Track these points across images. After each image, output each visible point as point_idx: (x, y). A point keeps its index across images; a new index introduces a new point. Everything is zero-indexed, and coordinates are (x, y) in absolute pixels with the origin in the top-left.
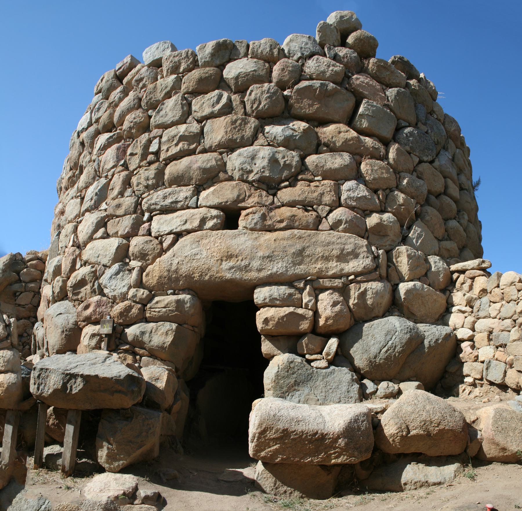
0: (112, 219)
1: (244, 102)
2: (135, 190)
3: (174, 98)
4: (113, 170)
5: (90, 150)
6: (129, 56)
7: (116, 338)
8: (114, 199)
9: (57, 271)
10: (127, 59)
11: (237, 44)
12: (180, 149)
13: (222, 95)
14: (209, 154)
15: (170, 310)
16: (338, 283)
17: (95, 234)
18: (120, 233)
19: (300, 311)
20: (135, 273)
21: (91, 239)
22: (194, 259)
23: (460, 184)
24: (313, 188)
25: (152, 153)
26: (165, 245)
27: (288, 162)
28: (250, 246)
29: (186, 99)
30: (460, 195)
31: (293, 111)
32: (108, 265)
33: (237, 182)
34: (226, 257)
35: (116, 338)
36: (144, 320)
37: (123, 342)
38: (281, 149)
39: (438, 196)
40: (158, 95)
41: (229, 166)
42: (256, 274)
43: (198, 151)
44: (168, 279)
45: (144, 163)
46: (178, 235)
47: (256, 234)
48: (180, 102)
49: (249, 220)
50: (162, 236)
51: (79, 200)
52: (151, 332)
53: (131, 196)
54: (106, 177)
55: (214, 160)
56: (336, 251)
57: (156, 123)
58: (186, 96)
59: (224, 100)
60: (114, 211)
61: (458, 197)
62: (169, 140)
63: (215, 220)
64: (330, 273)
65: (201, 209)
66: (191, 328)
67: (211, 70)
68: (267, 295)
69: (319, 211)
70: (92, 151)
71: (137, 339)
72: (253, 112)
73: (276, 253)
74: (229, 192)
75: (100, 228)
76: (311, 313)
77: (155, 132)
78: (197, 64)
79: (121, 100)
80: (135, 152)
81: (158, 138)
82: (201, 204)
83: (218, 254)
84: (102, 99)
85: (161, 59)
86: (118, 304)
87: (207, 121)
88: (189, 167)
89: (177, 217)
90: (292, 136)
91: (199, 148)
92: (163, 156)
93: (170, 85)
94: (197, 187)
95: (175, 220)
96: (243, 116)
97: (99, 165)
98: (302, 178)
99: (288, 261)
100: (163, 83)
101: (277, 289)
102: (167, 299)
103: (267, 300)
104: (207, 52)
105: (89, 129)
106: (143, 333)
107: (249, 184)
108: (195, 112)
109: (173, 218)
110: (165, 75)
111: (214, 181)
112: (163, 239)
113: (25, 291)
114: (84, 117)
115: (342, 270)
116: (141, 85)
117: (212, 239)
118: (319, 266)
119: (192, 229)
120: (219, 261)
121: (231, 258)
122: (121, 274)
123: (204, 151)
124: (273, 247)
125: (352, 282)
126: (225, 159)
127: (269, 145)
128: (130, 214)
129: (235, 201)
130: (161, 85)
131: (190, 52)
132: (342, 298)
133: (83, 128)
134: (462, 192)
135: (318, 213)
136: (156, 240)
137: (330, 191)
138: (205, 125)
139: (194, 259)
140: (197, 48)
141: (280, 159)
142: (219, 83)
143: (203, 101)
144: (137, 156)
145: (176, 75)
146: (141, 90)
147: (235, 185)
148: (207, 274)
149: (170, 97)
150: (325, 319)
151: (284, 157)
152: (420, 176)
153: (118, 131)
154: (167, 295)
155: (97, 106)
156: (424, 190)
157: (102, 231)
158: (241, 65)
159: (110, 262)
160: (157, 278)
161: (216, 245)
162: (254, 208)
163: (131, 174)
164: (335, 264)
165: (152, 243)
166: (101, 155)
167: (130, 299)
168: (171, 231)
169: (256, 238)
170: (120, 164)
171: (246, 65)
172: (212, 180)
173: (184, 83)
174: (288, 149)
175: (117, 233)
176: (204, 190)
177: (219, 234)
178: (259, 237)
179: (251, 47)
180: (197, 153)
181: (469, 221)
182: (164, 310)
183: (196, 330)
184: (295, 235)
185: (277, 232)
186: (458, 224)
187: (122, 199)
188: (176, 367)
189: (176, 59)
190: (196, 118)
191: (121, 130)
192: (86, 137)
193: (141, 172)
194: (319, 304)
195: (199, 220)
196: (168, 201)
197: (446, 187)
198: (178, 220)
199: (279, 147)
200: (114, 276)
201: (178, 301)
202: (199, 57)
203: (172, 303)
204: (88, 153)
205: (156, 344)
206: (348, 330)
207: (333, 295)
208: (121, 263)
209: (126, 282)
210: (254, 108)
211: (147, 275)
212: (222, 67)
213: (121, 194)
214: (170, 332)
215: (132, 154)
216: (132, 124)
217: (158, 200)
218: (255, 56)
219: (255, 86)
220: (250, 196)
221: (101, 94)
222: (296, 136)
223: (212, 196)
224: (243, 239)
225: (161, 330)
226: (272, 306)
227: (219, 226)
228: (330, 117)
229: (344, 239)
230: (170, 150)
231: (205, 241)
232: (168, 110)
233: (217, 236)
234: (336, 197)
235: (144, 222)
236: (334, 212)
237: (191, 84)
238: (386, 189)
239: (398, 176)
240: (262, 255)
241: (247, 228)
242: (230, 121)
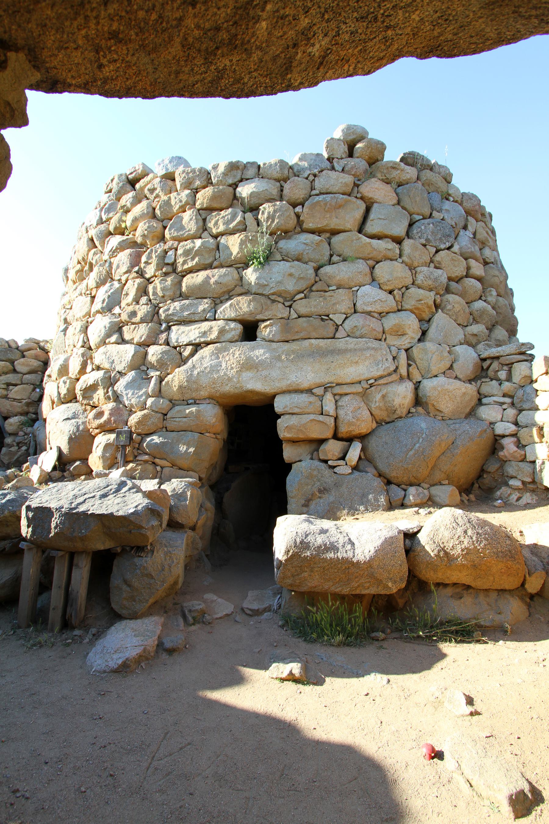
0: (127, 325)
9: (64, 370)
16: (358, 389)
20: (153, 381)
21: (103, 342)
23: (484, 260)
30: (485, 271)
31: (305, 226)
35: (134, 448)
37: (142, 453)
39: (458, 280)
46: (197, 347)
48: (194, 218)
50: (180, 346)
51: (89, 298)
53: (147, 304)
54: (119, 280)
59: (239, 219)
61: (483, 274)
66: (214, 436)
93: (184, 199)
95: (193, 331)
112: (182, 350)
113: (22, 384)
134: (487, 266)
152: (437, 265)
156: (444, 280)
161: (235, 357)
166: (113, 257)
175: (133, 339)
181: (499, 295)
183: (219, 436)
186: (485, 304)
187: (138, 306)
197: (468, 268)
202: (212, 176)
206: (370, 433)
213: (137, 301)
228: (342, 228)
238: (402, 287)
239: (414, 272)
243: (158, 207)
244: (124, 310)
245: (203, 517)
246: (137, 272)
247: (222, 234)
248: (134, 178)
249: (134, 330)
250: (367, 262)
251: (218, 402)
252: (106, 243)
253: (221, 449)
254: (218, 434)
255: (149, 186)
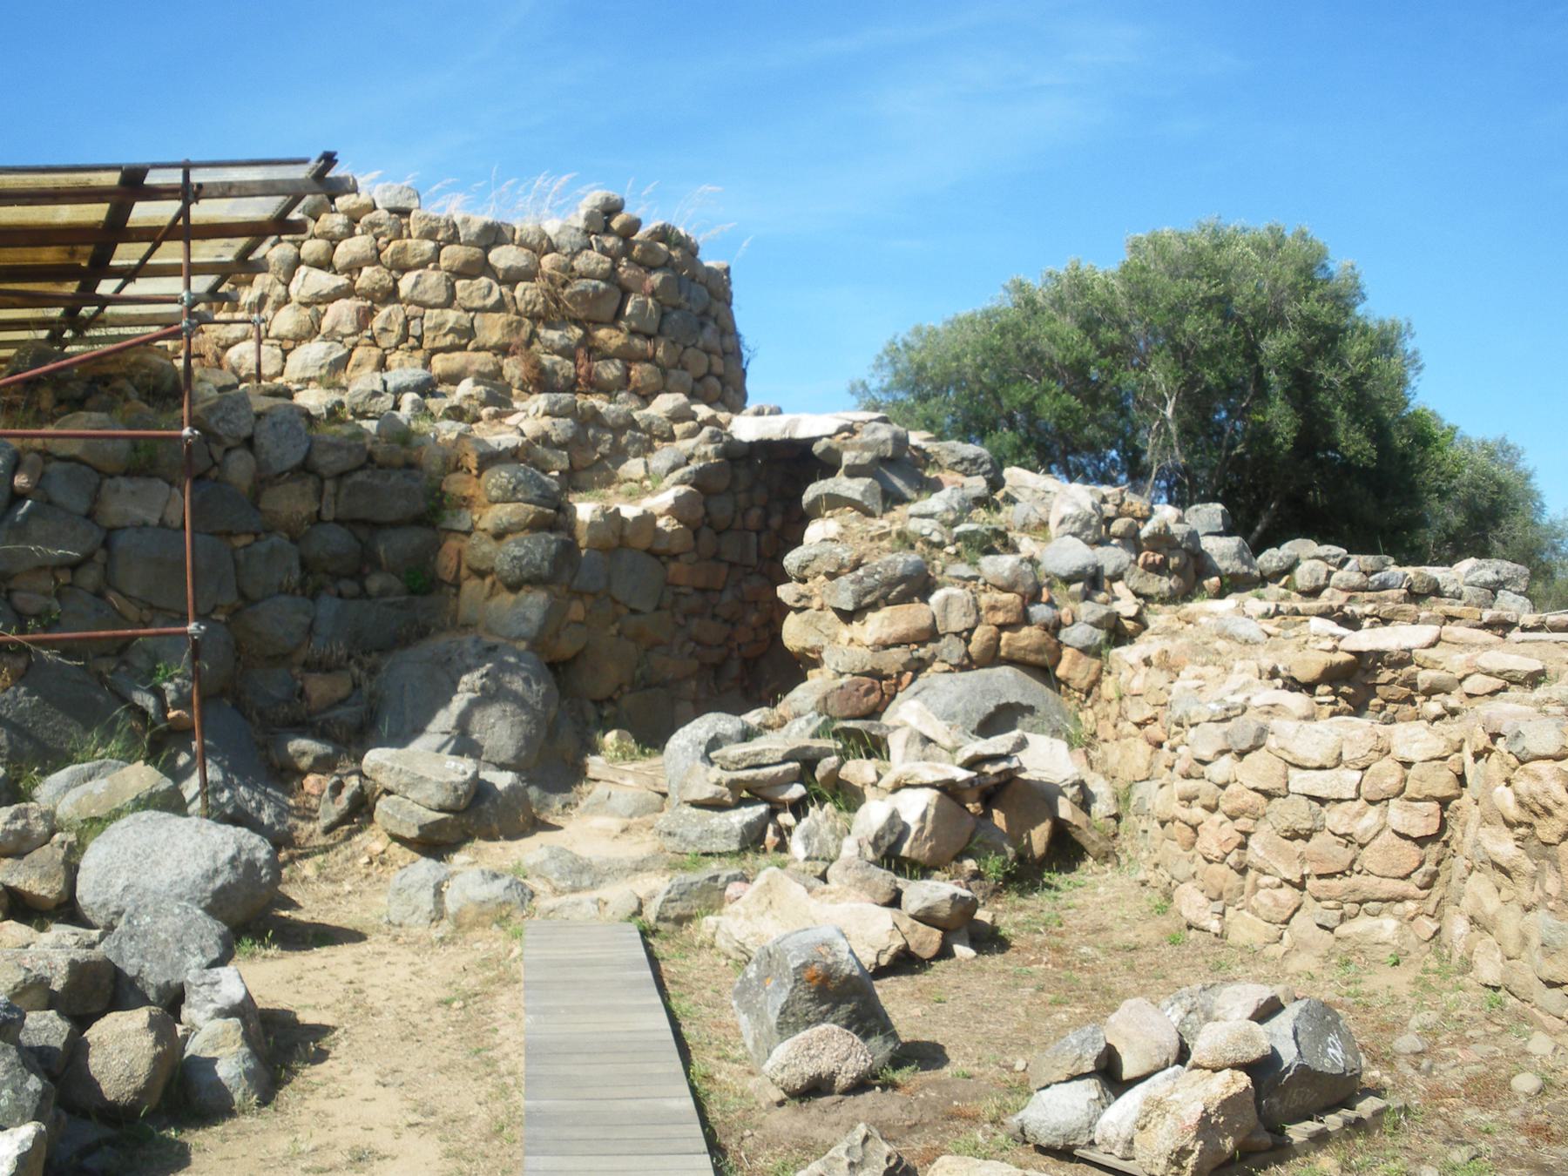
59: (495, 296)
92: (427, 344)
123: (477, 349)
189: (434, 224)
197: (710, 365)
212: (487, 249)
218: (523, 244)
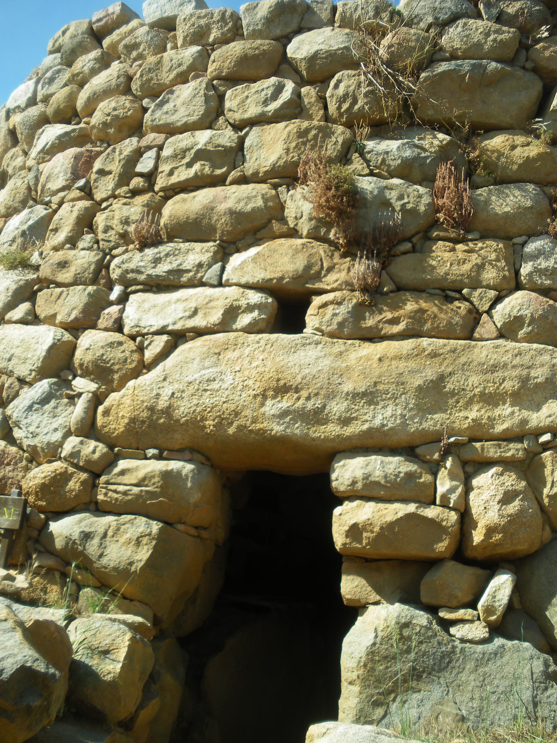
0: (48, 287)
1: (325, 99)
2: (100, 238)
3: (192, 84)
4: (62, 194)
5: (25, 147)
6: (119, 3)
7: (30, 538)
8: (56, 249)
10: (115, 9)
11: (314, 5)
12: (196, 173)
13: (284, 86)
14: (251, 186)
15: (147, 492)
17: (9, 311)
18: (59, 318)
19: (431, 512)
20: (81, 404)
22: (206, 390)
24: (461, 255)
25: (141, 175)
26: (149, 354)
27: (409, 206)
28: (326, 369)
29: (214, 88)
32: (27, 380)
33: (304, 240)
34: (274, 390)
35: (30, 538)
36: (92, 507)
37: (42, 549)
38: (396, 181)
40: (164, 75)
41: (290, 212)
42: (338, 428)
43: (229, 179)
44: (149, 426)
45: (122, 190)
47: (340, 345)
48: (202, 92)
49: (328, 317)
50: (143, 335)
52: (105, 535)
53: (90, 249)
55: (259, 197)
56: (511, 383)
57: (155, 123)
58: (215, 82)
59: (286, 95)
60: (53, 272)
62: (175, 156)
63: (256, 314)
64: (499, 428)
65: (227, 289)
66: (193, 532)
67: (264, 44)
68: (359, 474)
69: (475, 300)
70: (29, 150)
71: (72, 547)
72: (341, 115)
73: (381, 387)
74: (286, 259)
75: (22, 301)
76: (453, 516)
77: (151, 138)
78: (240, 32)
79: (94, 72)
80: (107, 169)
81: (155, 149)
82: (228, 280)
83: (258, 384)
84: (60, 64)
85: (175, 18)
86: (39, 464)
87: (251, 129)
88: (210, 209)
89: (178, 300)
90: (416, 158)
91: (234, 174)
92: (160, 182)
94: (225, 245)
95: (173, 307)
96: (322, 123)
97: (37, 179)
98: (437, 235)
99: (407, 404)
100: (174, 57)
101: (382, 462)
102: (145, 466)
103: (359, 485)
104: (259, 16)
105: (30, 109)
106: (87, 536)
107: (330, 245)
108: (230, 110)
109: (169, 302)
110: (179, 45)
111: (258, 236)
112: (146, 343)
114: (22, 87)
115: (524, 422)
116: (134, 54)
117: (247, 351)
118: (473, 414)
119: (206, 327)
120: (259, 399)
121: (287, 392)
122: (53, 403)
123: (243, 180)
124: (377, 374)
125: (545, 447)
126: (283, 197)
127: (371, 174)
128: (84, 283)
129: (300, 277)
130: (171, 60)
131: (228, 14)
132: (523, 483)
133: (18, 107)
135: (471, 303)
136: (132, 342)
137: (498, 260)
138: (247, 134)
139: (206, 390)
140: (242, 8)
141: (393, 201)
142: (279, 65)
143: (246, 94)
144: (111, 176)
145: (200, 48)
146: (133, 63)
147: (300, 247)
148: (232, 423)
149: (185, 81)
150: (484, 531)
151: (401, 197)
153: (82, 125)
154: (146, 458)
155: (49, 75)
157: (23, 309)
158: (320, 39)
159: (34, 373)
160: (126, 421)
161: (254, 364)
162: (338, 294)
163: (97, 207)
164: (510, 410)
165: (122, 348)
166: (43, 162)
167: (65, 459)
168: (164, 327)
169: (341, 353)
170: (76, 185)
171: (330, 38)
172: (255, 234)
173: (214, 61)
174: (410, 181)
175: (54, 316)
176: (238, 251)
177: (263, 343)
178: (347, 350)
179: (340, 10)
180: (228, 182)
182: (136, 490)
184: (424, 350)
185: (385, 343)
187: (73, 252)
188: (155, 616)
189: (202, 22)
190: (231, 121)
191: (87, 123)
192: (20, 123)
193: (114, 206)
194: (472, 496)
195: (222, 311)
196: (163, 268)
198: (180, 307)
199: (392, 177)
200: (36, 406)
201: (166, 475)
202: (244, 23)
203: (153, 477)
204: (21, 153)
205: (112, 564)
207: (505, 477)
208: (54, 380)
209: (59, 421)
210: (342, 110)
211: (107, 413)
214: (145, 540)
215: (102, 173)
216: (109, 118)
217: (142, 264)
218: (346, 23)
219: (346, 72)
220: (330, 269)
221: (59, 55)
222: (427, 157)
223: (251, 266)
224: (312, 353)
225: (125, 532)
226: (368, 499)
227: (262, 325)
229: (528, 357)
230: (176, 173)
231: (230, 355)
232: (179, 102)
233: (257, 346)
234: (509, 270)
235: (111, 304)
236: (507, 300)
237: (226, 64)
240: (351, 389)
241: (321, 331)
242: (295, 131)
243: (138, 75)
244: (47, 259)
245: (153, 706)
246: (81, 189)
247: (253, 122)
248: (103, 27)
249: (59, 298)
250: (545, 189)
251: (208, 459)
252: (36, 137)
253: (276, 314)
254: (205, 529)
255: (126, 41)
